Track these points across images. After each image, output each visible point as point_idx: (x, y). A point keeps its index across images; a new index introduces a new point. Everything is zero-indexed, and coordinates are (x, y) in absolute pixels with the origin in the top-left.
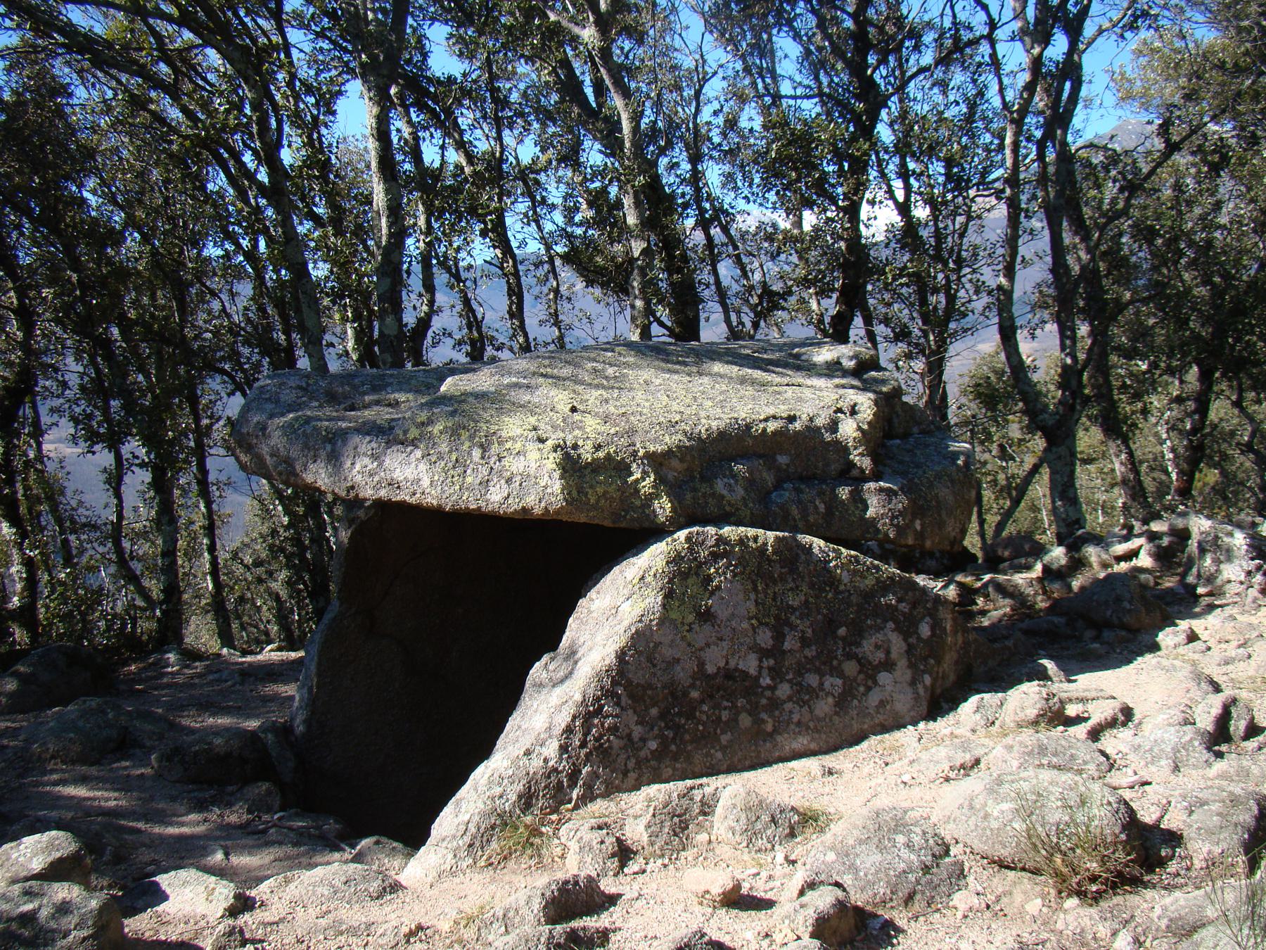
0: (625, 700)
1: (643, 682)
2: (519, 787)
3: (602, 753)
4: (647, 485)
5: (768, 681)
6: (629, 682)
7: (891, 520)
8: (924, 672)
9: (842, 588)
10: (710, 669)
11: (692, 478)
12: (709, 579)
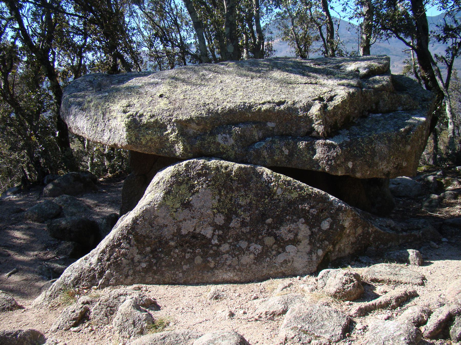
0: (133, 242)
1: (144, 234)
2: (77, 274)
3: (117, 265)
4: (172, 137)
5: (216, 242)
6: (137, 233)
7: (327, 162)
8: (319, 248)
9: (276, 197)
10: (184, 232)
11: (205, 133)
12: (193, 186)
